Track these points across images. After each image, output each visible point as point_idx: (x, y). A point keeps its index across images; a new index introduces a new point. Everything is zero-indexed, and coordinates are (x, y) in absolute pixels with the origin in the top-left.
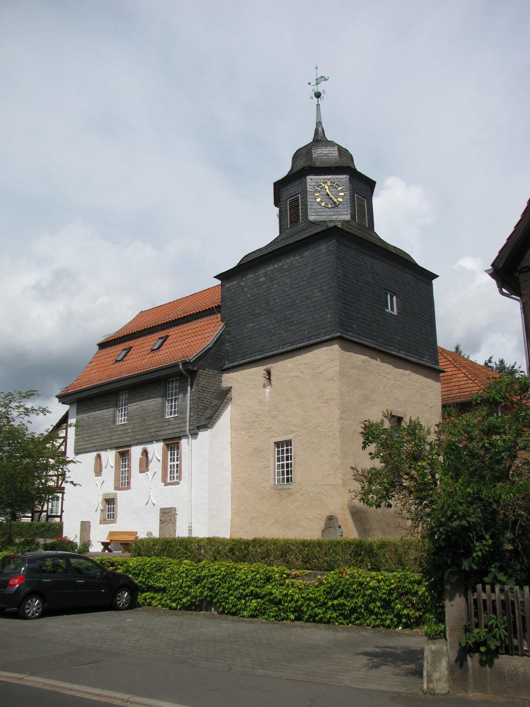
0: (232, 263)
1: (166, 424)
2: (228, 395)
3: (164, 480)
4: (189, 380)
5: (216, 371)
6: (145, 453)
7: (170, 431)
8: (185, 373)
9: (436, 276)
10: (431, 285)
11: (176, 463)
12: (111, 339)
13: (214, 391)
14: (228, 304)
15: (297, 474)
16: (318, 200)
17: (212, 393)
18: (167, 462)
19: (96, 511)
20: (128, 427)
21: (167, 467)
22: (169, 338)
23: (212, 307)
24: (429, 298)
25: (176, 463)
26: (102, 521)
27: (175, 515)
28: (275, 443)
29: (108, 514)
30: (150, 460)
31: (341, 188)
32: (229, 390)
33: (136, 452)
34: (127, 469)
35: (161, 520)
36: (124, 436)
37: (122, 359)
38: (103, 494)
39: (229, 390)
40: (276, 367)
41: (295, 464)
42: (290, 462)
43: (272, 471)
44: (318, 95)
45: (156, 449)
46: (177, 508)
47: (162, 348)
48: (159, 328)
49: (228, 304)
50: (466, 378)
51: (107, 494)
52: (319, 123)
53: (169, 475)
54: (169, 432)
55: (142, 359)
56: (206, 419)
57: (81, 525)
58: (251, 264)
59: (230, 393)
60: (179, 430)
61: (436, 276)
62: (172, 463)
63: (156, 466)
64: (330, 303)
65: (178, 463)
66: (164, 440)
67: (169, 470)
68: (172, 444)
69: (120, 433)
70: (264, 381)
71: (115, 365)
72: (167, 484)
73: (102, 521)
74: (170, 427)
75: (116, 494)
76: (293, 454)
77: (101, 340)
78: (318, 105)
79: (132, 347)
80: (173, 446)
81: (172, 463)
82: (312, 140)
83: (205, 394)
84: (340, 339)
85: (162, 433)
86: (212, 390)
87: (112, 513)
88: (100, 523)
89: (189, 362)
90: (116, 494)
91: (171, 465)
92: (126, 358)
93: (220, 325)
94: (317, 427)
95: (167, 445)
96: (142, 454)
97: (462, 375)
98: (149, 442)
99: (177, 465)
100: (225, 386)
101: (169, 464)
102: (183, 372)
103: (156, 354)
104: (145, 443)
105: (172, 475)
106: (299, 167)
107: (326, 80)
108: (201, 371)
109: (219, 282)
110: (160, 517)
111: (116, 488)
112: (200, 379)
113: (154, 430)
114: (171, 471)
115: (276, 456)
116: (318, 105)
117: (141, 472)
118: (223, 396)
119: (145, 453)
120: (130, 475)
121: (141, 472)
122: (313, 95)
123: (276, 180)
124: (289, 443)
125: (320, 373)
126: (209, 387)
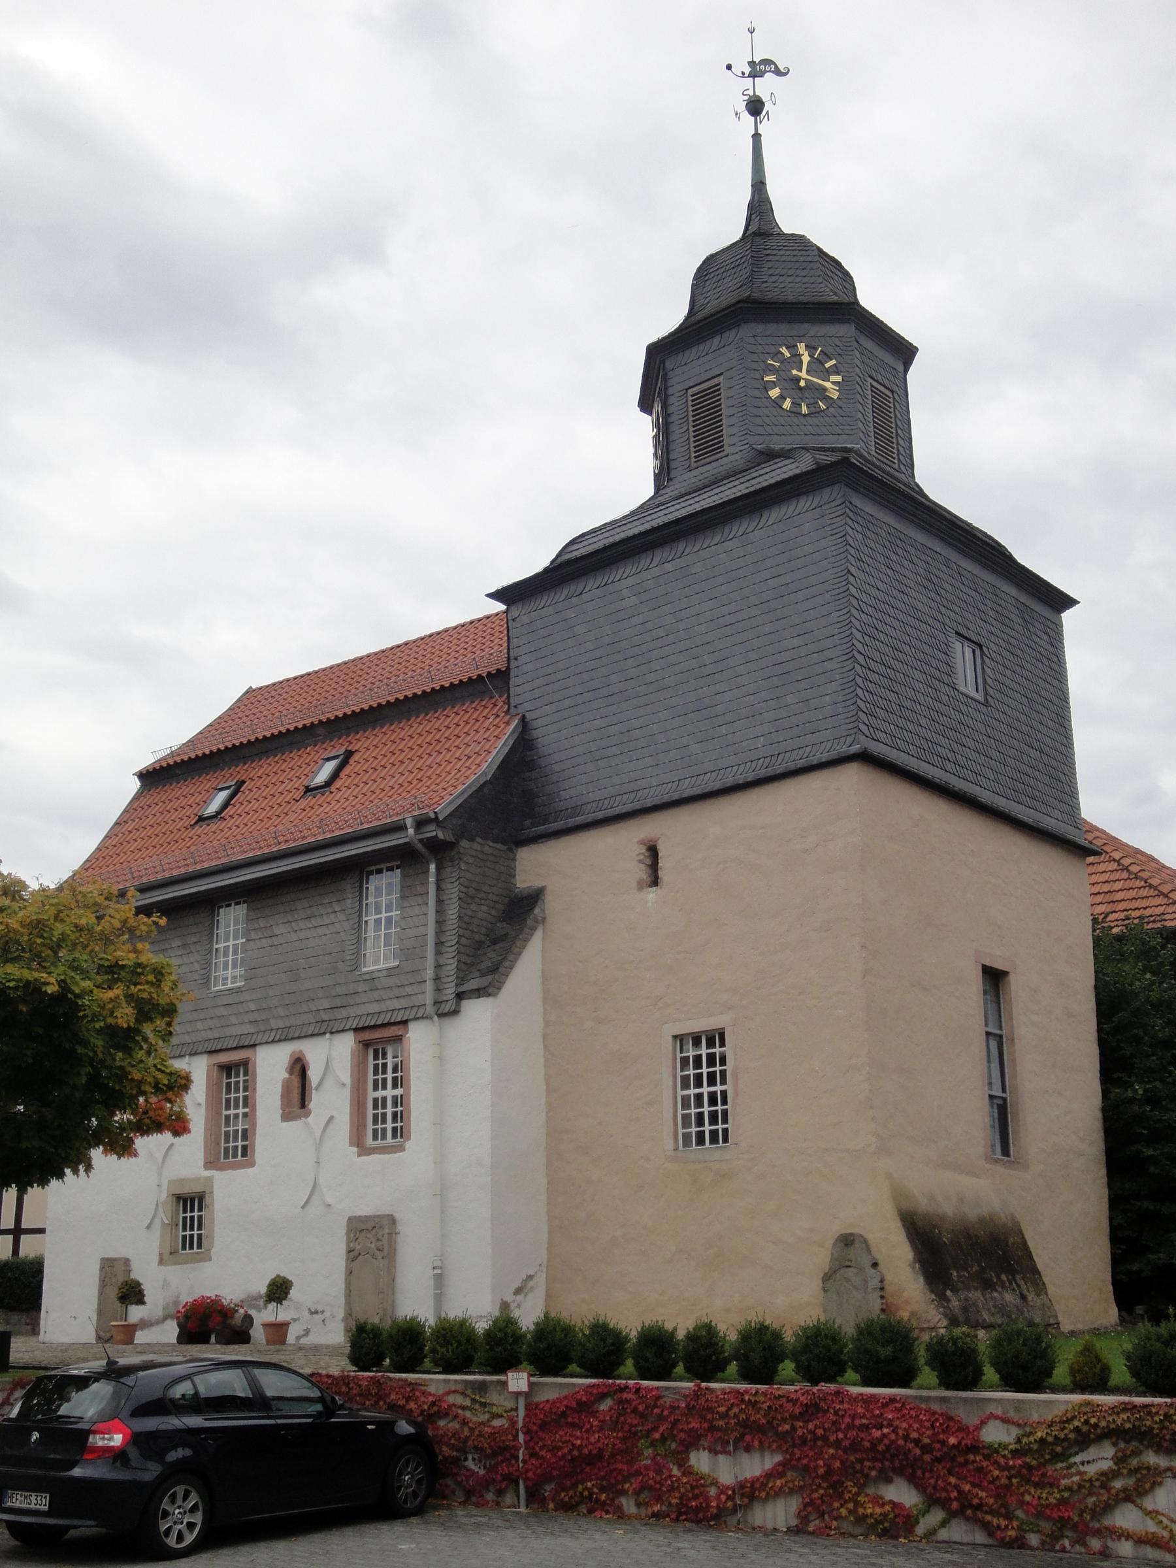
0: (534, 559)
1: (362, 987)
2: (537, 911)
3: (357, 1140)
4: (432, 867)
5: (499, 846)
6: (299, 1068)
7: (375, 1008)
8: (424, 851)
9: (1069, 602)
10: (1058, 626)
11: (390, 1093)
12: (178, 759)
13: (495, 898)
14: (527, 668)
15: (744, 1119)
16: (774, 393)
17: (492, 904)
18: (365, 1090)
19: (148, 1227)
20: (245, 996)
21: (365, 1103)
22: (356, 757)
23: (480, 676)
24: (1055, 659)
25: (390, 1093)
26: (166, 1257)
27: (393, 1234)
28: (675, 1037)
29: (184, 1237)
30: (314, 1085)
31: (834, 362)
32: (534, 898)
33: (270, 1066)
34: (241, 1111)
35: (349, 1251)
36: (234, 1020)
37: (218, 813)
38: (170, 1182)
39: (534, 898)
40: (674, 832)
41: (736, 1094)
42: (719, 1088)
43: (668, 1114)
44: (755, 107)
45: (333, 1058)
46: (397, 1216)
47: (338, 783)
48: (321, 731)
49: (527, 668)
50: (1125, 875)
51: (182, 1181)
52: (759, 186)
53: (370, 1126)
54: (370, 1008)
55: (275, 818)
56: (484, 974)
57: (102, 1268)
58: (583, 565)
59: (539, 904)
60: (402, 1003)
61: (1069, 602)
62: (380, 1094)
63: (332, 1099)
64: (829, 665)
65: (399, 1091)
66: (356, 1030)
67: (370, 1112)
68: (379, 1040)
69: (223, 1011)
70: (643, 874)
71: (198, 830)
72: (364, 1151)
73: (166, 1256)
74: (376, 995)
75: (209, 1180)
76: (729, 1067)
77: (146, 760)
78: (757, 137)
79: (244, 782)
80: (380, 1047)
81: (380, 1094)
82: (737, 235)
83: (473, 907)
84: (866, 758)
85: (352, 1011)
86: (490, 896)
87: (196, 1232)
88: (161, 1262)
89: (437, 818)
90: (209, 1180)
91: (375, 1100)
92: (230, 810)
93: (508, 723)
94: (800, 994)
95: (366, 1044)
96: (291, 1070)
97: (1114, 866)
98: (312, 1035)
99: (395, 1098)
100: (525, 885)
101: (372, 1095)
102: (419, 846)
103: (320, 799)
104: (299, 1038)
105: (382, 1122)
106: (715, 302)
107: (778, 72)
108: (464, 844)
109: (502, 607)
110: (349, 1241)
111: (210, 1164)
112: (463, 866)
113: (326, 1004)
114: (375, 1116)
115: (679, 1073)
116: (757, 137)
117: (287, 1117)
118: (521, 911)
119: (299, 1068)
120: (254, 1125)
121: (287, 1117)
122: (742, 107)
123: (653, 339)
124: (716, 1037)
125: (805, 851)
126: (485, 888)
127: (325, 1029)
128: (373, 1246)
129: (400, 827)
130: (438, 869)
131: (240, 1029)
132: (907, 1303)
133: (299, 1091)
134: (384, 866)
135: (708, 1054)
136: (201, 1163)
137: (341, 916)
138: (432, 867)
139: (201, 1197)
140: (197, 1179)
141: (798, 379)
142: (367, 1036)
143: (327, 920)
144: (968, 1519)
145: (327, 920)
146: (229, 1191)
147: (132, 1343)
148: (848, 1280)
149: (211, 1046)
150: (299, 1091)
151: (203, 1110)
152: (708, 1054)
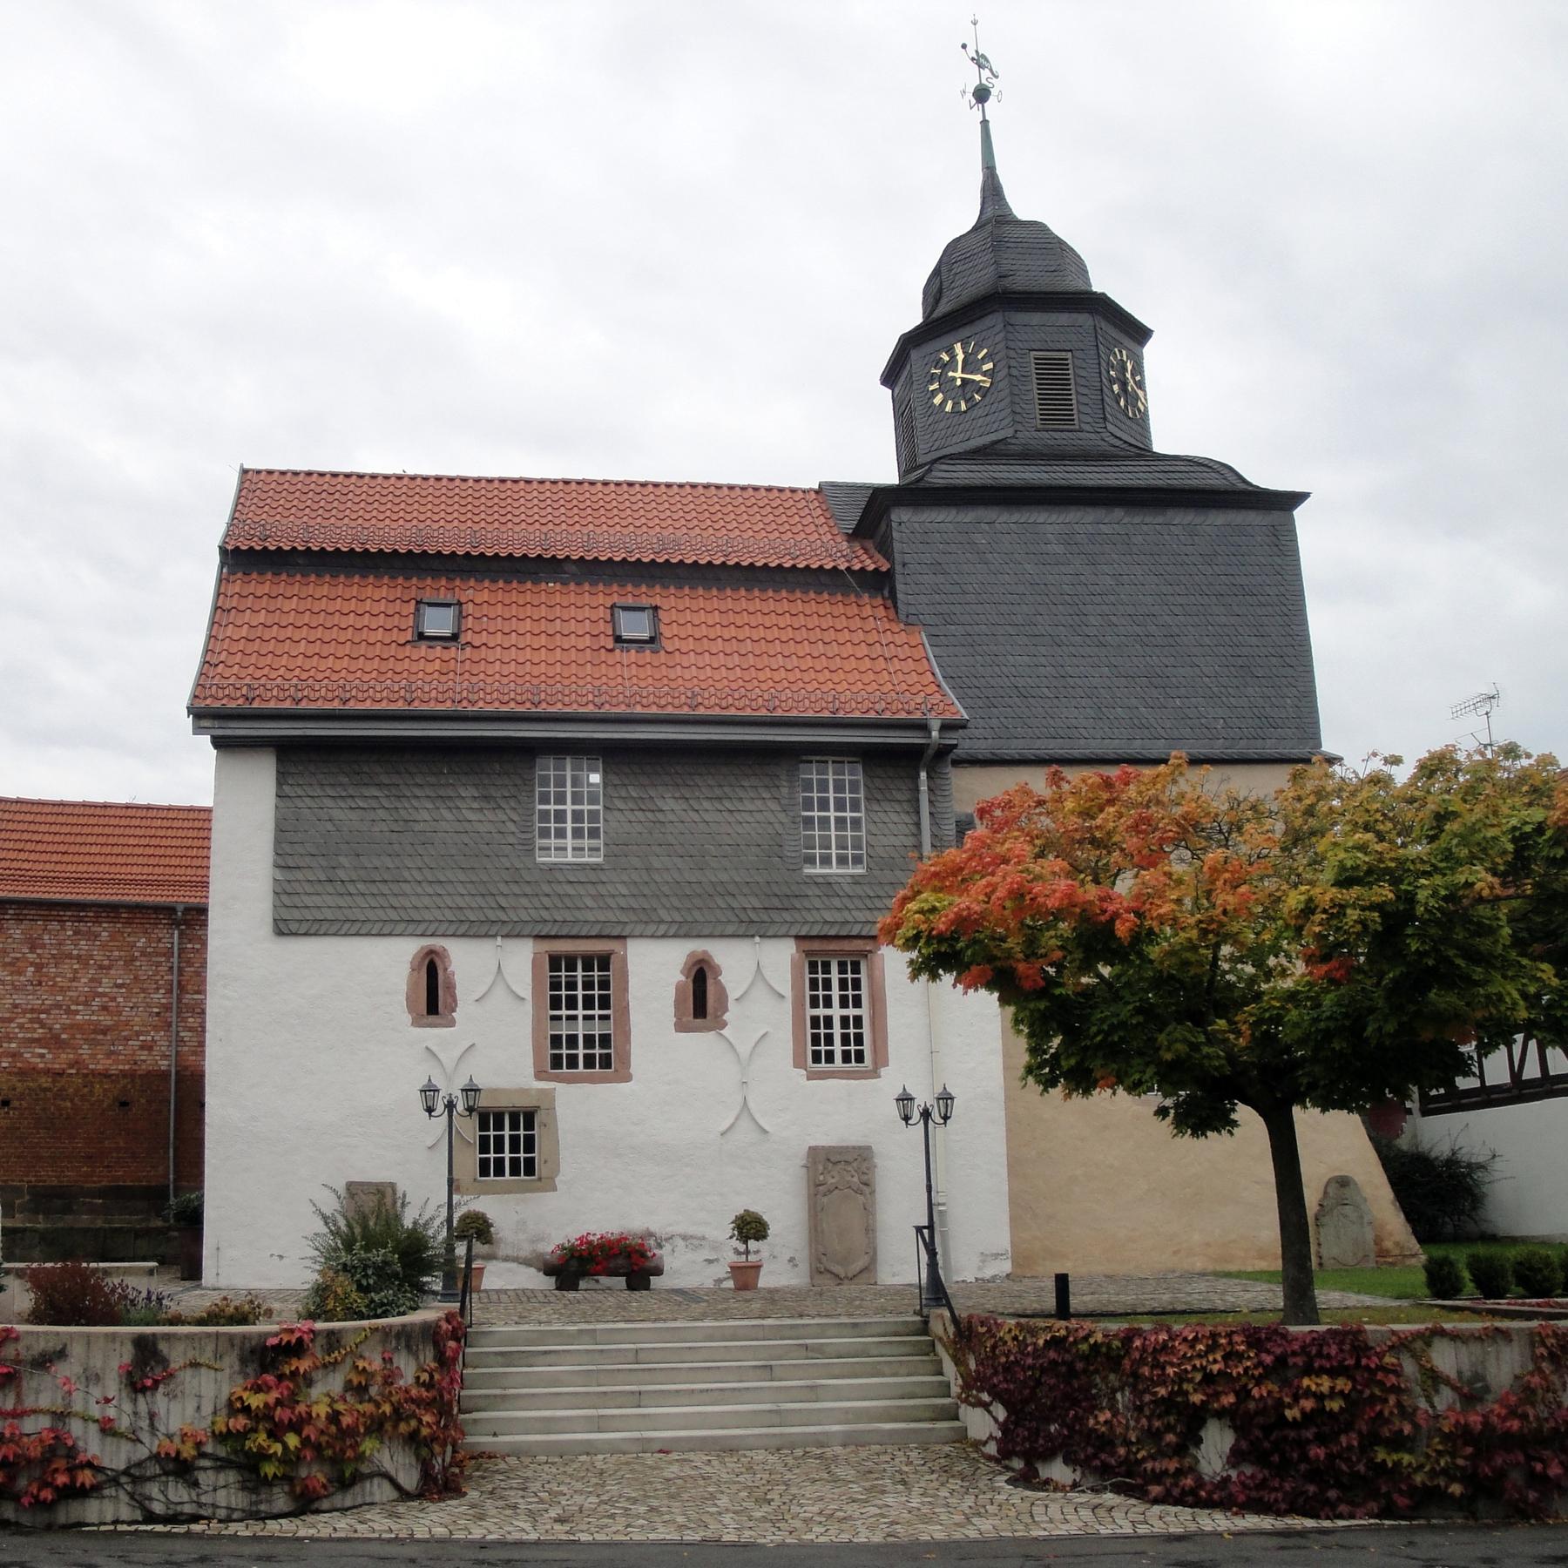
54: (826, 917)
66: (797, 937)
75: (549, 1095)
78: (985, 123)
116: (985, 123)
127: (750, 928)
128: (855, 1179)
129: (923, 727)
130: (929, 777)
131: (858, 919)
132: (1391, 1234)
133: (700, 998)
134: (814, 758)
135: (576, 1008)
136: (531, 1071)
137: (773, 806)
138: (923, 775)
139: (529, 1117)
140: (524, 1092)
141: (954, 379)
142: (816, 946)
143: (751, 807)
144: (418, 1456)
145: (749, 806)
146: (578, 1110)
147: (755, 1287)
148: (1345, 1216)
149: (538, 929)
150: (700, 998)
151: (528, 1007)
152: (576, 1008)
